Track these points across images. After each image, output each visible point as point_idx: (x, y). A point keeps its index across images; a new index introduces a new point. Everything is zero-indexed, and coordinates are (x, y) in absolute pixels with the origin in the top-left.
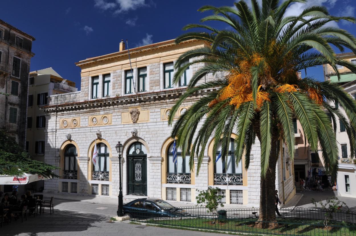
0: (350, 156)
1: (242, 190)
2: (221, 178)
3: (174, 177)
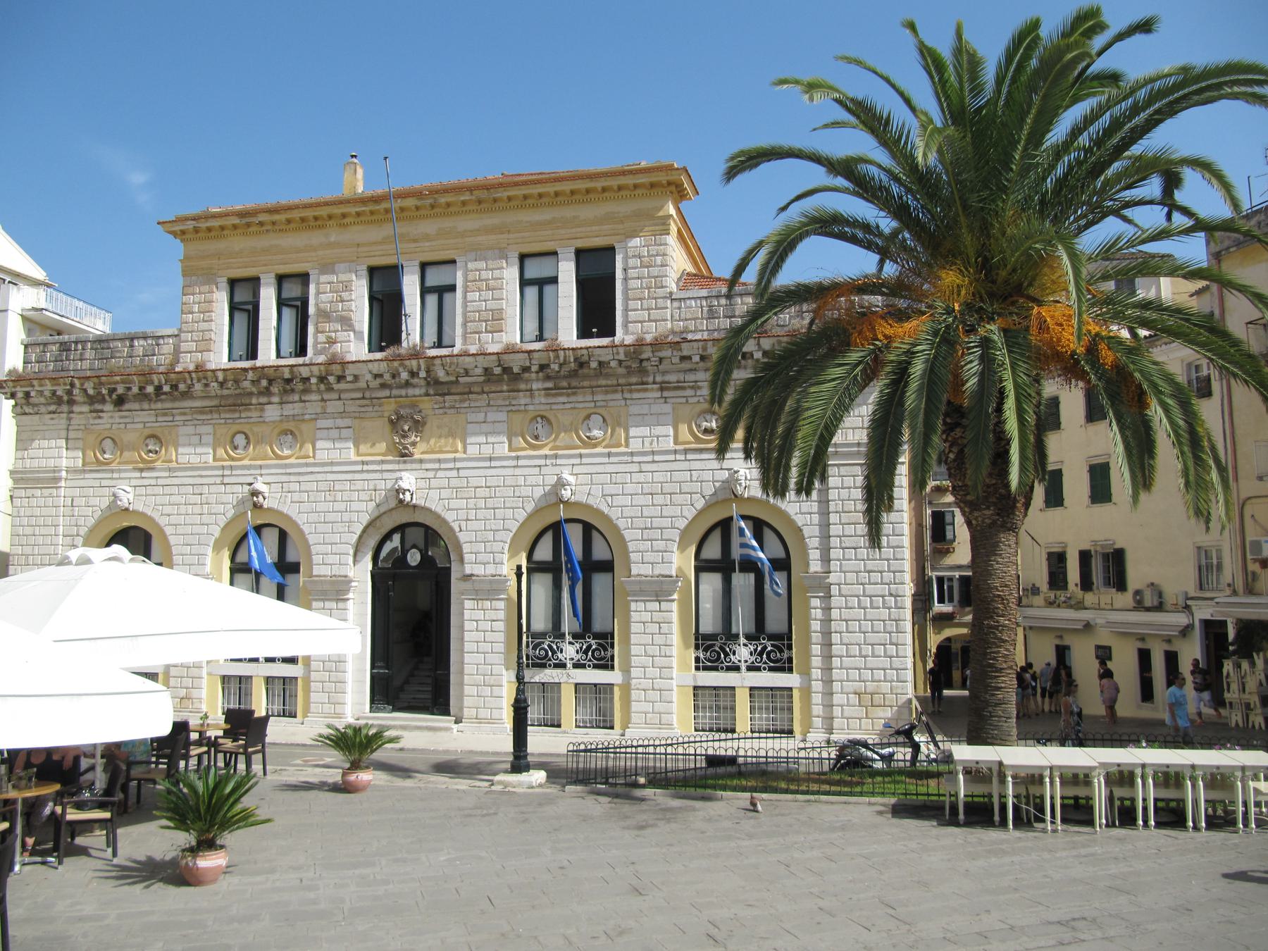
0: (1076, 585)
1: (733, 688)
2: (717, 649)
3: (550, 647)
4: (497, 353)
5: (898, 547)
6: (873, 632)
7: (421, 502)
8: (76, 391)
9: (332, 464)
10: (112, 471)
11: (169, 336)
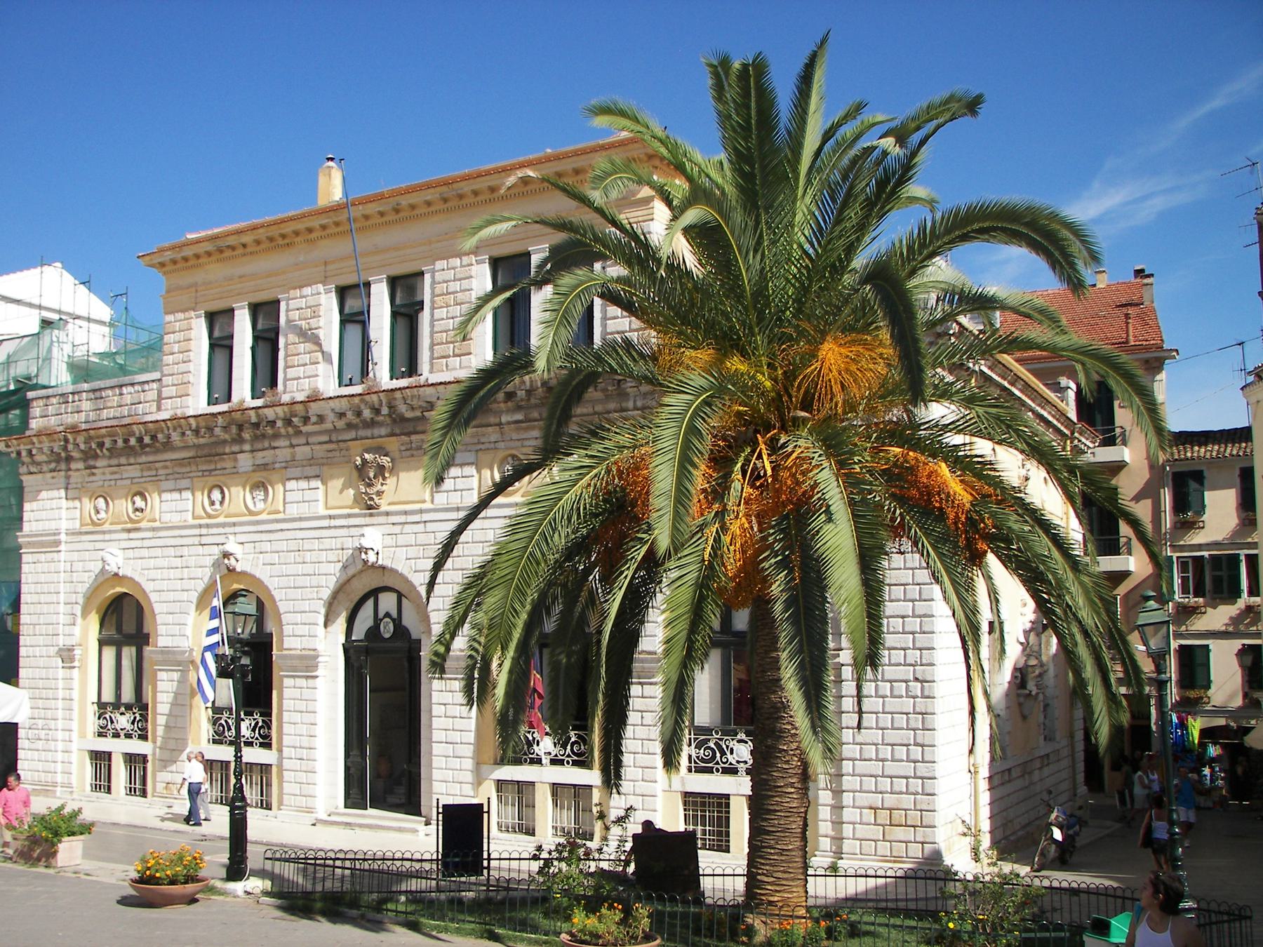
2: (713, 746)
4: (360, 395)
5: (925, 616)
6: (893, 728)
7: (388, 563)
8: (70, 447)
9: (301, 519)
10: (104, 532)
11: (153, 381)
